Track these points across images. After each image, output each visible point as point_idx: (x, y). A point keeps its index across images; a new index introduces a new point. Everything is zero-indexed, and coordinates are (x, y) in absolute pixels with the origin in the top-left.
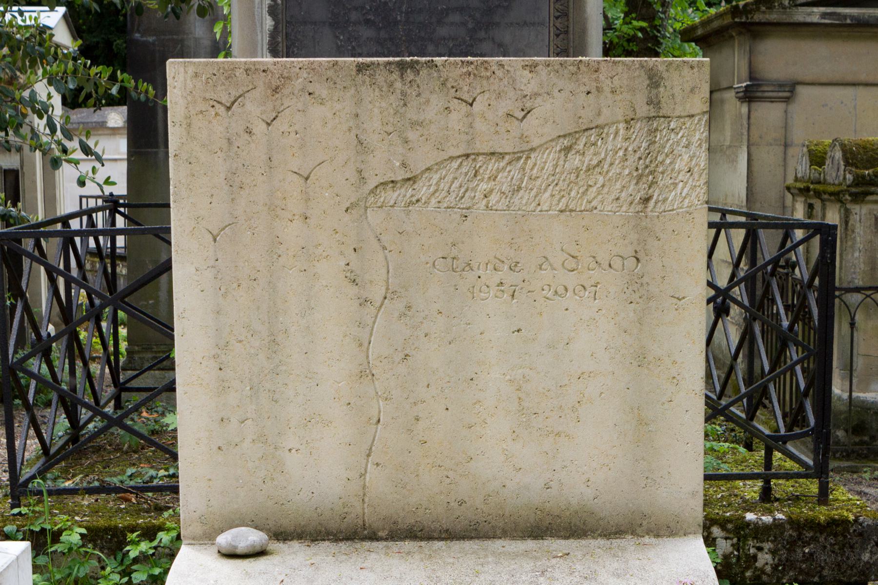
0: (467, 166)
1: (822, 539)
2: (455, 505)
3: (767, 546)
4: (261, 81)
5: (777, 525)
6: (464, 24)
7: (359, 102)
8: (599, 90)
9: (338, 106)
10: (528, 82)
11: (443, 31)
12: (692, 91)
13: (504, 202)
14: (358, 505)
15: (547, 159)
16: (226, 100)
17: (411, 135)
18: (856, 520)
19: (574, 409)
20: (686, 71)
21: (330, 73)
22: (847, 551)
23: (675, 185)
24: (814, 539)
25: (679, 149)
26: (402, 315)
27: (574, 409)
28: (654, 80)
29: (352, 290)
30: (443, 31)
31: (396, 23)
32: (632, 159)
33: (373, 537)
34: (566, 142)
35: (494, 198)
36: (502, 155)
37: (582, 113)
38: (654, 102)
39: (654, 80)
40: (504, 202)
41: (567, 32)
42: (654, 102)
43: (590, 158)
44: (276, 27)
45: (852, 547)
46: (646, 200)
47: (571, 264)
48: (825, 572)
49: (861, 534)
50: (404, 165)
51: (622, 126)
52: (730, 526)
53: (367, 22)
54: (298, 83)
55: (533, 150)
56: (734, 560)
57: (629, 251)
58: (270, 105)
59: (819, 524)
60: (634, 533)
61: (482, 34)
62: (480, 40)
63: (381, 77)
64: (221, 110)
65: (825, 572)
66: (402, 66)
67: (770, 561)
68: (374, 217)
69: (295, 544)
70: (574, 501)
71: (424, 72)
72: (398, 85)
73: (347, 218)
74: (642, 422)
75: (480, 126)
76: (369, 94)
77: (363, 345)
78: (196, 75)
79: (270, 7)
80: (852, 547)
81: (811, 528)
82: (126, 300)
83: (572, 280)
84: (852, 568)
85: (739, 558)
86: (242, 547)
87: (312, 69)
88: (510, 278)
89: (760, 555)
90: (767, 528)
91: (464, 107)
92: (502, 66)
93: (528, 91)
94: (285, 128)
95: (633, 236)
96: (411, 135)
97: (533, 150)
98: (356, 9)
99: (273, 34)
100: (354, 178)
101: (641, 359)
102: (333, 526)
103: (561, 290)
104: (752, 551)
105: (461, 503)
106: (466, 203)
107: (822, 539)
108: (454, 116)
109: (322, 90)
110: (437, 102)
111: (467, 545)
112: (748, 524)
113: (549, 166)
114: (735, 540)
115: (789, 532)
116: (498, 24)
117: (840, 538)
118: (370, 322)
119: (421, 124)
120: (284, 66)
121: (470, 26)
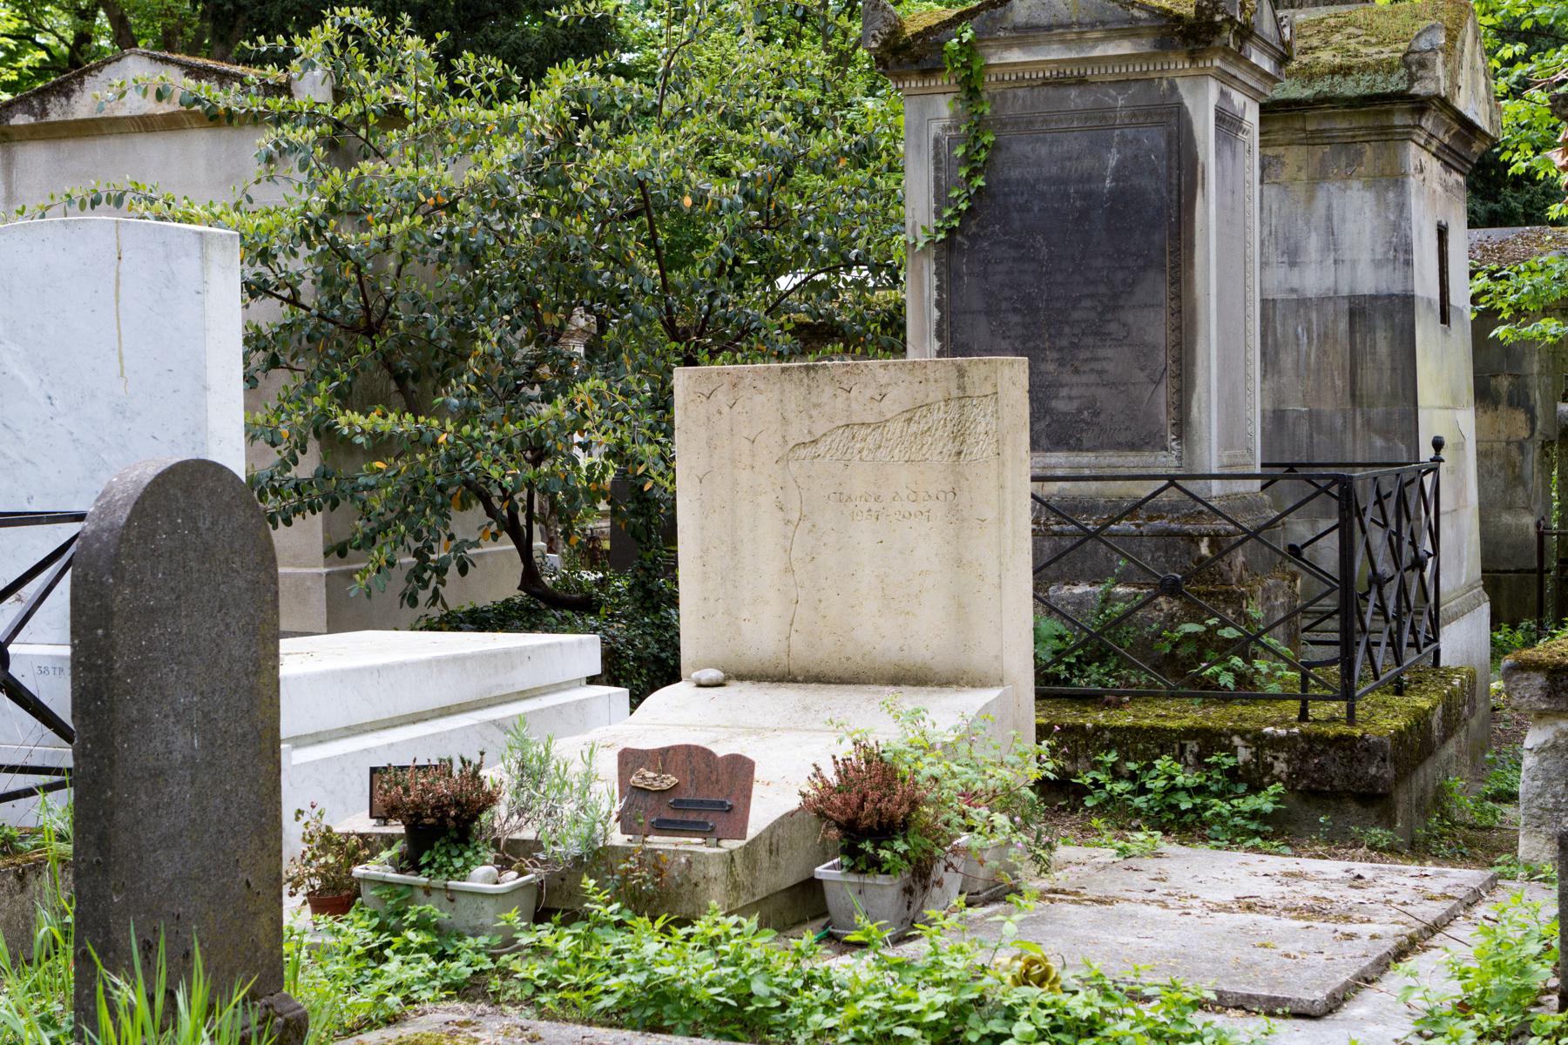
0: (848, 432)
1: (1331, 752)
2: (843, 660)
3: (1282, 756)
4: (726, 379)
5: (1290, 738)
6: (1094, 308)
7: (783, 392)
8: (927, 380)
9: (771, 395)
10: (883, 376)
11: (1076, 315)
12: (985, 379)
13: (871, 456)
14: (785, 658)
15: (896, 427)
16: (707, 393)
17: (814, 413)
18: (1362, 737)
19: (917, 596)
20: (981, 366)
21: (766, 374)
22: (1356, 765)
23: (978, 443)
24: (1323, 751)
25: (979, 418)
26: (810, 531)
27: (917, 596)
28: (961, 373)
29: (780, 515)
30: (1076, 315)
31: (1038, 309)
32: (949, 425)
33: (794, 680)
34: (908, 415)
35: (865, 453)
36: (869, 425)
37: (916, 395)
38: (962, 388)
39: (961, 373)
40: (871, 456)
41: (1180, 312)
42: (962, 388)
43: (923, 426)
44: (941, 317)
45: (1359, 761)
46: (959, 453)
47: (913, 497)
48: (1336, 783)
49: (1367, 750)
50: (810, 432)
51: (942, 404)
52: (1248, 736)
53: (1015, 310)
54: (747, 381)
55: (887, 421)
56: (1252, 766)
57: (948, 488)
58: (731, 396)
59: (1327, 739)
60: (958, 684)
61: (1109, 316)
62: (1109, 321)
63: (796, 375)
64: (704, 399)
65: (1336, 783)
66: (808, 368)
67: (1285, 769)
68: (794, 466)
69: (747, 683)
70: (919, 660)
71: (820, 372)
72: (806, 380)
73: (777, 466)
74: (961, 606)
75: (854, 406)
76: (788, 386)
77: (788, 551)
78: (690, 377)
79: (937, 301)
80: (1359, 761)
81: (1321, 742)
82: (1328, 587)
83: (913, 508)
84: (1360, 779)
85: (1257, 764)
86: (703, 681)
87: (755, 371)
88: (875, 506)
89: (1276, 764)
90: (1281, 740)
91: (845, 394)
92: (867, 366)
93: (883, 382)
94: (740, 410)
95: (952, 478)
96: (814, 413)
97: (887, 421)
98: (1005, 299)
99: (939, 323)
100: (780, 441)
101: (959, 562)
102: (771, 671)
103: (907, 515)
104: (1269, 759)
105: (848, 659)
106: (848, 456)
107: (1331, 752)
108: (839, 400)
109: (761, 385)
110: (829, 391)
111: (851, 687)
112: (1264, 736)
113: (898, 431)
114: (1254, 749)
115: (1302, 745)
116: (1122, 307)
117: (1348, 752)
118: (791, 535)
119: (819, 405)
120: (739, 370)
121: (1099, 309)
